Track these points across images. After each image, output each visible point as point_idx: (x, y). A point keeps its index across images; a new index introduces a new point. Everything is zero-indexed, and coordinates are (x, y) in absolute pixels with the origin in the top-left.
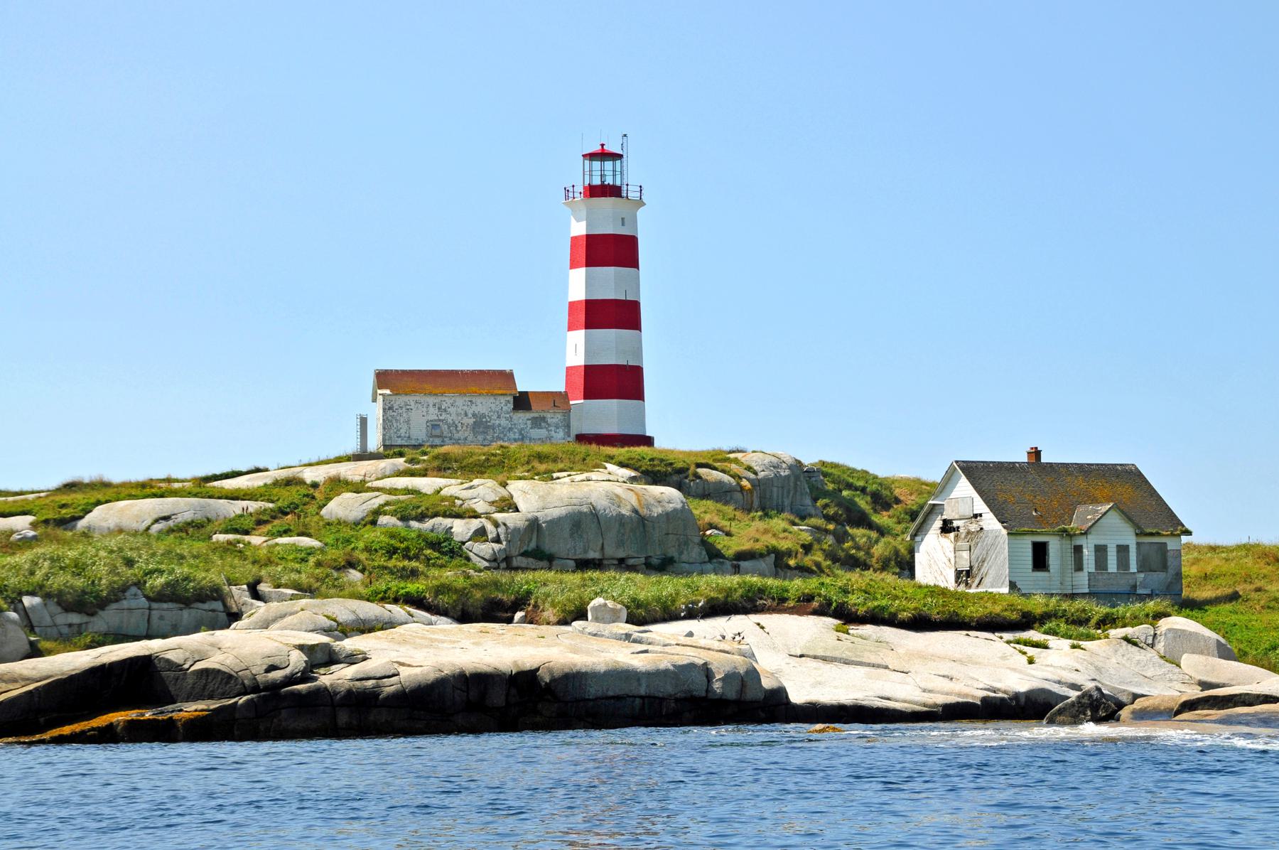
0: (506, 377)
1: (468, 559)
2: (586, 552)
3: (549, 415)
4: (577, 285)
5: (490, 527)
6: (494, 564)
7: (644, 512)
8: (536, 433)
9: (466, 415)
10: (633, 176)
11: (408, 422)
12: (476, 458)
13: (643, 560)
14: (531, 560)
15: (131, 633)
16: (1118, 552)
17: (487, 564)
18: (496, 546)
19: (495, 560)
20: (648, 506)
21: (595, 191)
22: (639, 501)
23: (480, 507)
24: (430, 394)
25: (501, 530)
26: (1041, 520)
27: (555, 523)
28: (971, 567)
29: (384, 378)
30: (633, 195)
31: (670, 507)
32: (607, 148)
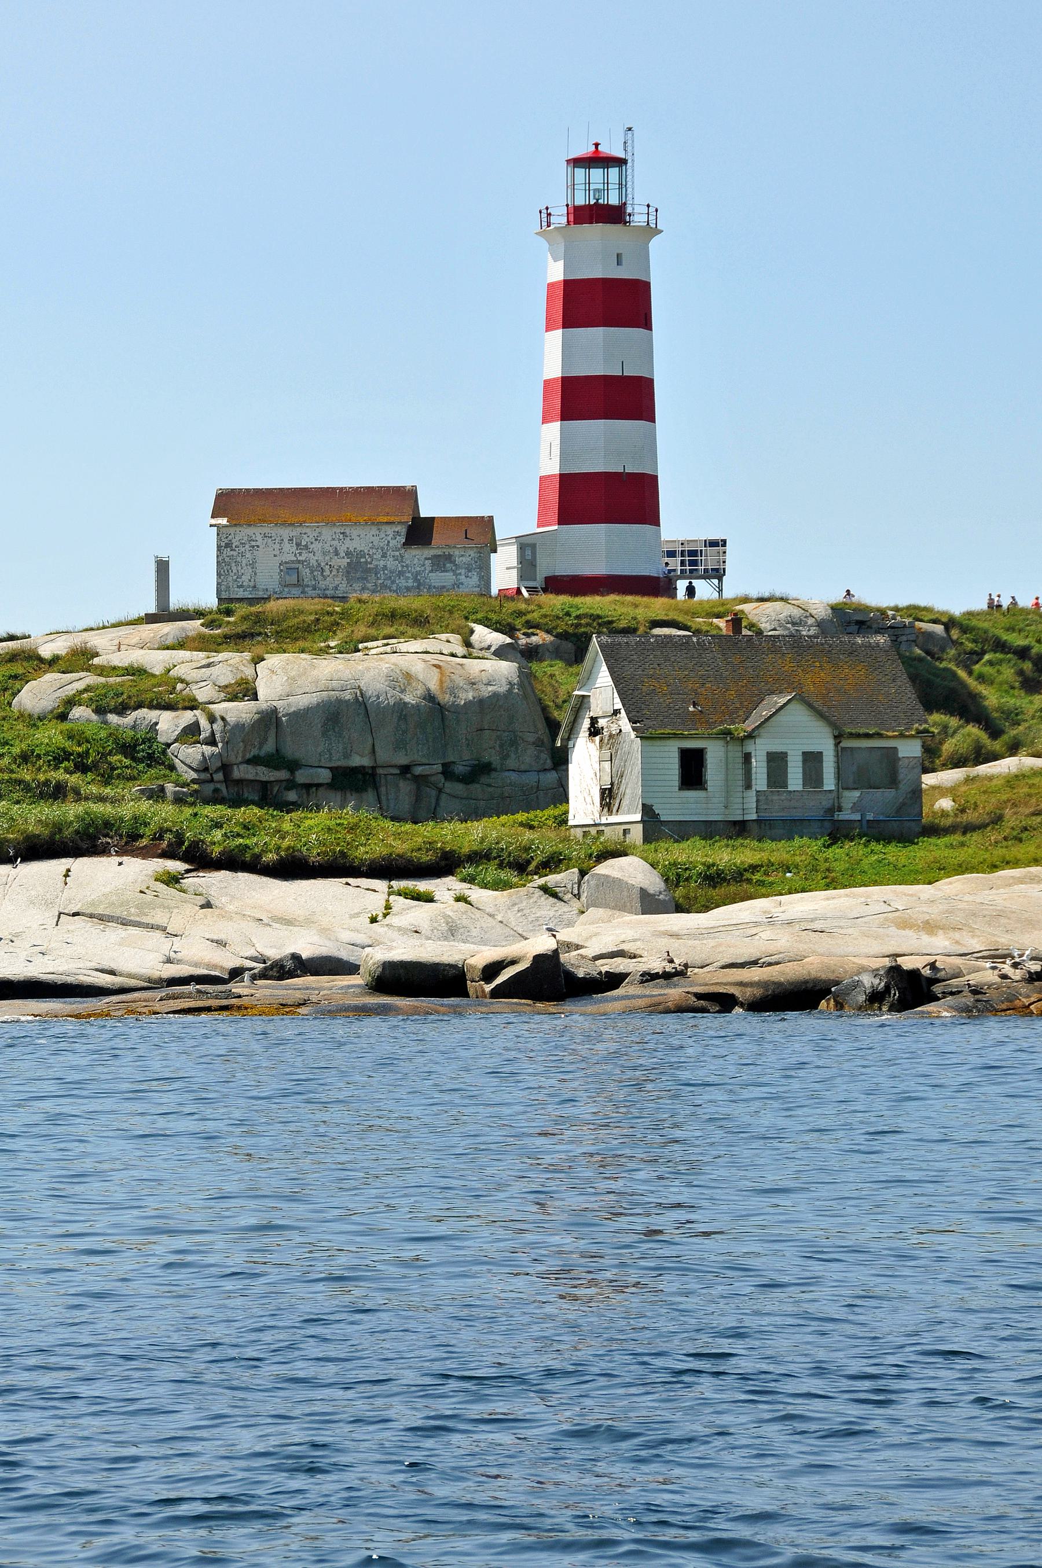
0: (408, 496)
1: (172, 768)
2: (347, 756)
3: (457, 553)
4: (551, 354)
5: (204, 723)
6: (205, 776)
7: (446, 699)
8: (439, 578)
9: (337, 553)
10: (643, 192)
11: (253, 564)
12: (301, 618)
13: (439, 768)
14: (261, 769)
15: (314, 857)
16: (805, 761)
17: (194, 775)
18: (208, 750)
19: (206, 769)
20: (453, 691)
21: (581, 215)
22: (441, 682)
23: (202, 694)
24: (285, 524)
25: (218, 727)
26: (694, 720)
27: (300, 716)
28: (612, 784)
29: (228, 503)
30: (639, 219)
31: (487, 691)
32: (605, 149)
